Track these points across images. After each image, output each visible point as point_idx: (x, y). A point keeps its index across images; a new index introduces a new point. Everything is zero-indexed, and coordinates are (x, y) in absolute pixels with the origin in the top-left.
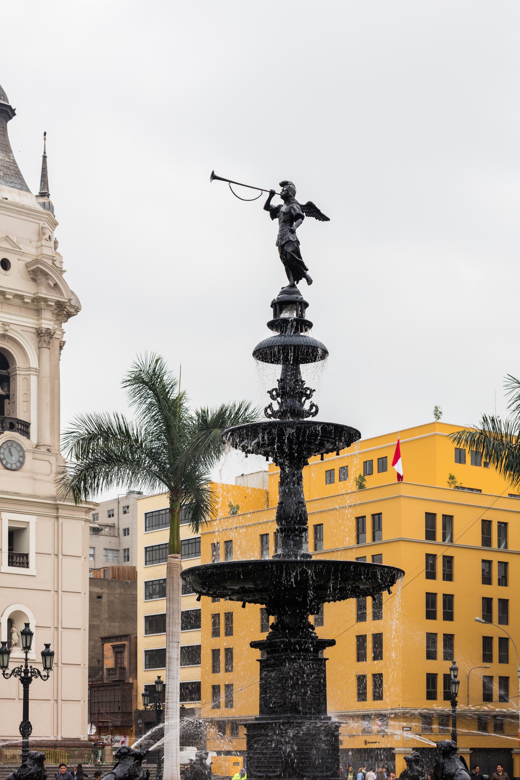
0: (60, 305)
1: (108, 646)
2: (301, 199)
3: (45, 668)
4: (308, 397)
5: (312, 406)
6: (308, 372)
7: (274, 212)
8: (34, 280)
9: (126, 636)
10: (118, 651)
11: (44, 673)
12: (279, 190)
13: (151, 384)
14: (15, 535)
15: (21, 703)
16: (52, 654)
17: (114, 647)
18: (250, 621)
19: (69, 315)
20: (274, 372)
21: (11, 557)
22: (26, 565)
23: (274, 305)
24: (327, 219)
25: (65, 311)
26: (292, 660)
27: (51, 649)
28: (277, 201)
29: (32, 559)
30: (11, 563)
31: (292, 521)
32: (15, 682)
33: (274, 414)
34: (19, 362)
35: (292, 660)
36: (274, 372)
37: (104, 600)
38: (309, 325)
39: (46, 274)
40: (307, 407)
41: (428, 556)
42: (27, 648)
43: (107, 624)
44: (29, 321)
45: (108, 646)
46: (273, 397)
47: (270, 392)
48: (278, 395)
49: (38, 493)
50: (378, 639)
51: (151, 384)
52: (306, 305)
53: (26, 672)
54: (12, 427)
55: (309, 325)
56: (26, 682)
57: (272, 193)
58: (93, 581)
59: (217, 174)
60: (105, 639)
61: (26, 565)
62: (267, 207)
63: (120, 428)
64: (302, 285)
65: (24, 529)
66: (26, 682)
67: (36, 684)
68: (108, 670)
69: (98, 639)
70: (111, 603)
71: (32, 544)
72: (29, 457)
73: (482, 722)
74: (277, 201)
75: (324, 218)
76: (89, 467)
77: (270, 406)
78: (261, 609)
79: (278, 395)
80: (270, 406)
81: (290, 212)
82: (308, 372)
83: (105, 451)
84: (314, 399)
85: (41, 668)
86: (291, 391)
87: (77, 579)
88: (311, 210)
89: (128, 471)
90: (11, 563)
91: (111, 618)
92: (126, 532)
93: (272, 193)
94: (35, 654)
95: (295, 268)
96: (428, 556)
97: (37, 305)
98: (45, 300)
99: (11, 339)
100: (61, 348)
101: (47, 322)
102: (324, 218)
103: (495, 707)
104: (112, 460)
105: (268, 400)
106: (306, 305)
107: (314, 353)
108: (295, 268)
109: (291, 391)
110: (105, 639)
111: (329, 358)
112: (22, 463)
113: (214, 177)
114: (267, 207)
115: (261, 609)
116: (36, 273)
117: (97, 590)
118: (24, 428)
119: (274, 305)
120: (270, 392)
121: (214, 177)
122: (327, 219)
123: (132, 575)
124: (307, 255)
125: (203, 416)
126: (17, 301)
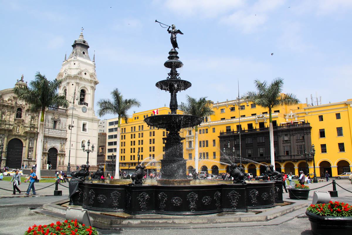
0: (95, 82)
1: (100, 148)
2: (177, 29)
3: (92, 150)
4: (178, 75)
5: (179, 77)
7: (170, 32)
8: (91, 77)
9: (104, 146)
10: (102, 149)
11: (92, 151)
12: (171, 26)
13: (116, 95)
14: (84, 125)
15: (89, 157)
16: (94, 147)
17: (102, 148)
18: (160, 133)
19: (97, 84)
20: (169, 70)
21: (83, 129)
22: (86, 131)
23: (170, 53)
24: (183, 34)
25: (96, 83)
26: (173, 142)
27: (94, 146)
28: (171, 29)
29: (87, 130)
30: (83, 131)
31: (174, 106)
32: (86, 153)
34: (87, 92)
35: (173, 142)
36: (169, 70)
37: (100, 139)
39: (93, 76)
41: (163, 132)
42: (89, 145)
43: (100, 144)
44: (90, 85)
45: (100, 148)
46: (169, 75)
47: (168, 74)
48: (170, 75)
49: (89, 117)
50: (154, 147)
51: (116, 95)
53: (88, 151)
54: (85, 104)
56: (88, 153)
57: (170, 27)
58: (99, 135)
59: (157, 21)
60: (100, 147)
61: (86, 131)
62: (168, 30)
63: (109, 102)
65: (86, 124)
66: (88, 153)
67: (90, 153)
68: (101, 152)
69: (99, 146)
70: (101, 140)
71: (87, 127)
72: (87, 110)
76: (103, 109)
77: (168, 77)
79: (170, 75)
80: (168, 77)
81: (174, 32)
83: (105, 107)
84: (179, 76)
86: (173, 74)
87: (96, 134)
88: (179, 32)
90: (83, 131)
91: (101, 143)
92: (104, 127)
93: (170, 27)
95: (175, 44)
96: (163, 132)
97: (91, 82)
98: (93, 81)
99: (86, 87)
100: (95, 90)
101: (93, 85)
104: (107, 108)
105: (168, 76)
107: (179, 65)
108: (175, 44)
109: (173, 74)
110: (100, 147)
112: (86, 111)
113: (156, 21)
116: (91, 76)
117: (99, 137)
118: (87, 104)
120: (168, 74)
121: (156, 21)
122: (183, 34)
123: (105, 134)
125: (126, 101)
126: (87, 81)
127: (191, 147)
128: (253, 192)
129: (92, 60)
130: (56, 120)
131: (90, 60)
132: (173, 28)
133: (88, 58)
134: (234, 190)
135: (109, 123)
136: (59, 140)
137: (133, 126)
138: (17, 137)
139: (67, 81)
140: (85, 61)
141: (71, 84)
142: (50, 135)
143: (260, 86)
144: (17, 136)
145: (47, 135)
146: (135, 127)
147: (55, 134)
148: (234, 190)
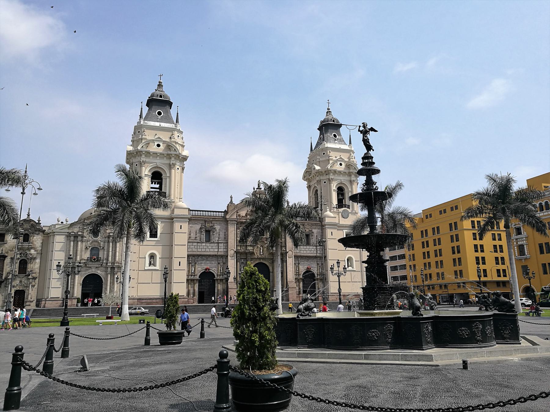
2: (369, 127)
6: (374, 178)
7: (361, 132)
23: (363, 158)
28: (362, 129)
32: (336, 277)
33: (365, 190)
38: (374, 163)
40: (374, 187)
42: (338, 267)
52: (372, 157)
55: (374, 163)
56: (530, 279)
57: (360, 126)
62: (359, 131)
64: (371, 152)
66: (339, 276)
67: (342, 278)
73: (498, 283)
74: (362, 129)
75: (376, 131)
78: (390, 250)
82: (374, 178)
85: (343, 272)
86: (369, 183)
88: (372, 129)
89: (530, 207)
93: (360, 126)
94: (341, 269)
95: (369, 148)
102: (376, 131)
103: (502, 279)
106: (372, 157)
109: (369, 183)
111: (381, 174)
114: (359, 131)
115: (390, 250)
119: (363, 158)
124: (371, 143)
127: (524, 254)
128: (476, 325)
129: (348, 143)
130: (308, 233)
131: (345, 144)
132: (364, 127)
133: (342, 141)
134: (389, 323)
135: (156, 237)
136: (315, 260)
137: (435, 227)
138: (262, 261)
139: (318, 178)
140: (338, 147)
141: (323, 182)
142: (302, 255)
143: (492, 179)
144: (262, 259)
145: (299, 254)
146: (426, 231)
147: (309, 252)
148: (389, 323)
